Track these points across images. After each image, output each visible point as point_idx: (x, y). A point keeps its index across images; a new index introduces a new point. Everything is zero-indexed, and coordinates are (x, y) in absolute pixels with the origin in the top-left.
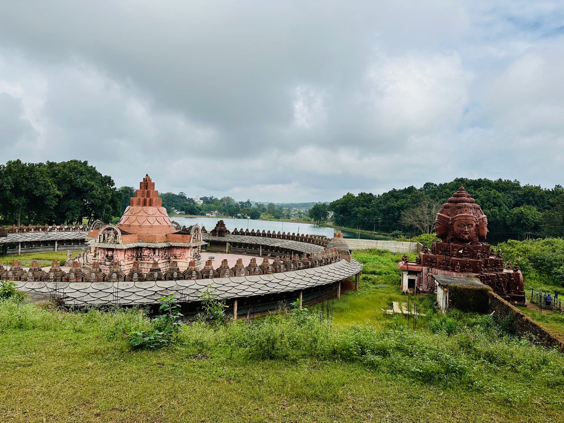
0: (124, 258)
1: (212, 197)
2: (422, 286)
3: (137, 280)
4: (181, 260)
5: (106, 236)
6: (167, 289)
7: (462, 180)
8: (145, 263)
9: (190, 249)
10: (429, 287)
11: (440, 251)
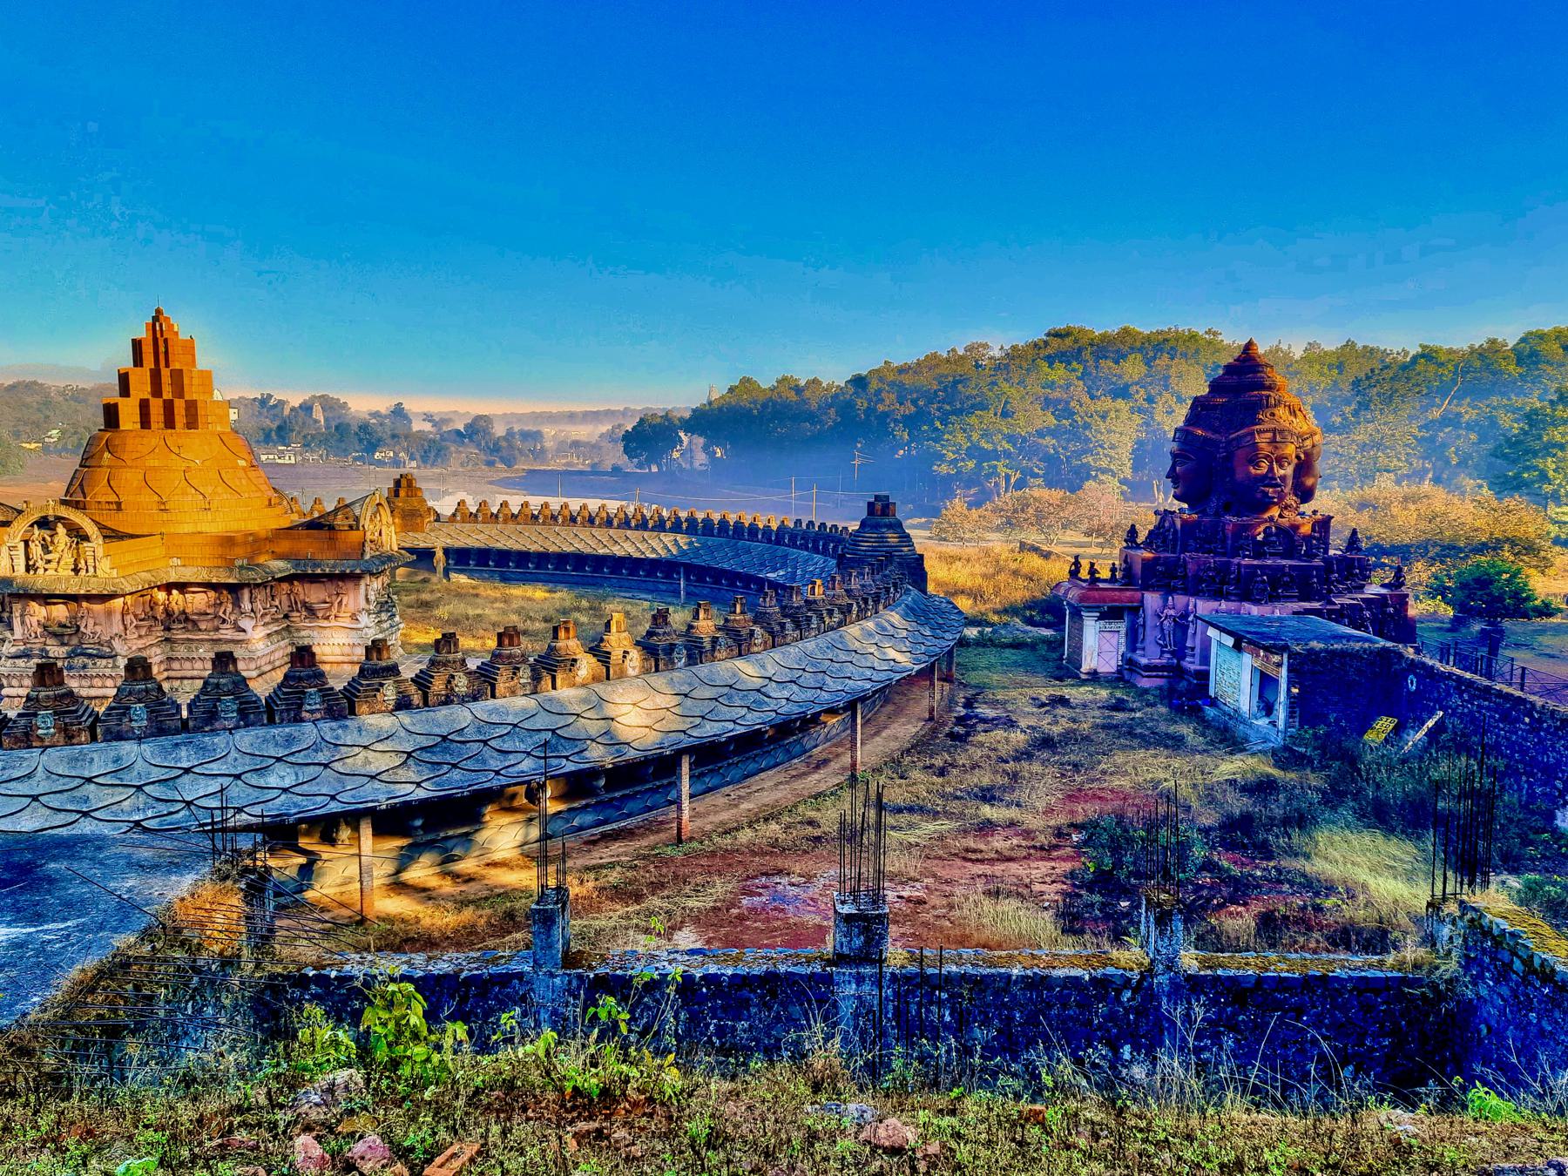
0: (122, 627)
1: (270, 396)
2: (1143, 649)
3: (318, 716)
4: (333, 623)
5: (36, 550)
6: (444, 738)
7: (1531, 333)
8: (202, 640)
9: (363, 583)
10: (1168, 652)
11: (1191, 542)
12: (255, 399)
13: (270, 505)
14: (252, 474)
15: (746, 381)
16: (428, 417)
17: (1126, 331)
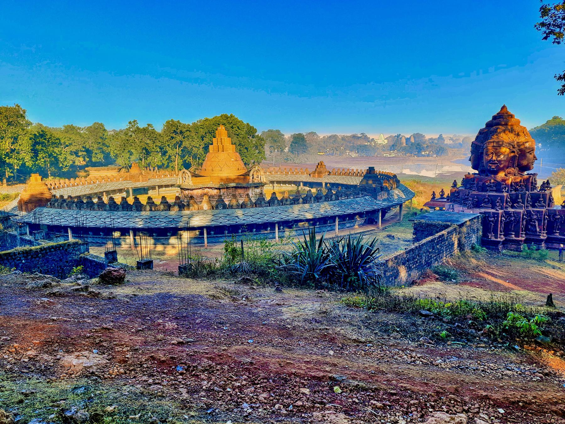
12: (395, 136)
13: (238, 169)
14: (235, 163)
15: (555, 118)
16: (451, 139)
17: (206, 120)
